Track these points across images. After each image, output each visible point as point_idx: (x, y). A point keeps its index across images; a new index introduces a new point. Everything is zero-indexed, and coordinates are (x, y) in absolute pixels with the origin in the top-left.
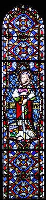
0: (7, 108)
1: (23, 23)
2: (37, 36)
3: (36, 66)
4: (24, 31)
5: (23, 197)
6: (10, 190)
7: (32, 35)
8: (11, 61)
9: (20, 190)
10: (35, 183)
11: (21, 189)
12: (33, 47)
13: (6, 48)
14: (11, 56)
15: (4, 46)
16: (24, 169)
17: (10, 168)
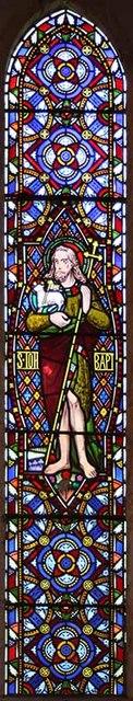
1: (66, 156)
4: (63, 130)
7: (91, 600)
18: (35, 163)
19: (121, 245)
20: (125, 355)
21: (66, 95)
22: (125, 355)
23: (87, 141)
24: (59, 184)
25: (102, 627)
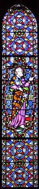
0: (7, 99)
1: (19, 20)
2: (31, 162)
3: (30, 35)
4: (20, 184)
5: (19, 54)
6: (7, 176)
7: (27, 161)
8: (9, 56)
9: (17, 151)
10: (30, 170)
11: (19, 153)
12: (28, 42)
13: (5, 132)
14: (9, 26)
15: (4, 169)
16: (20, 157)
17: (7, 26)
18: (10, 23)
19: (36, 67)
20: (37, 103)
21: (19, 144)
22: (37, 103)
23: (26, 171)
24: (17, 29)
25: (31, 169)
